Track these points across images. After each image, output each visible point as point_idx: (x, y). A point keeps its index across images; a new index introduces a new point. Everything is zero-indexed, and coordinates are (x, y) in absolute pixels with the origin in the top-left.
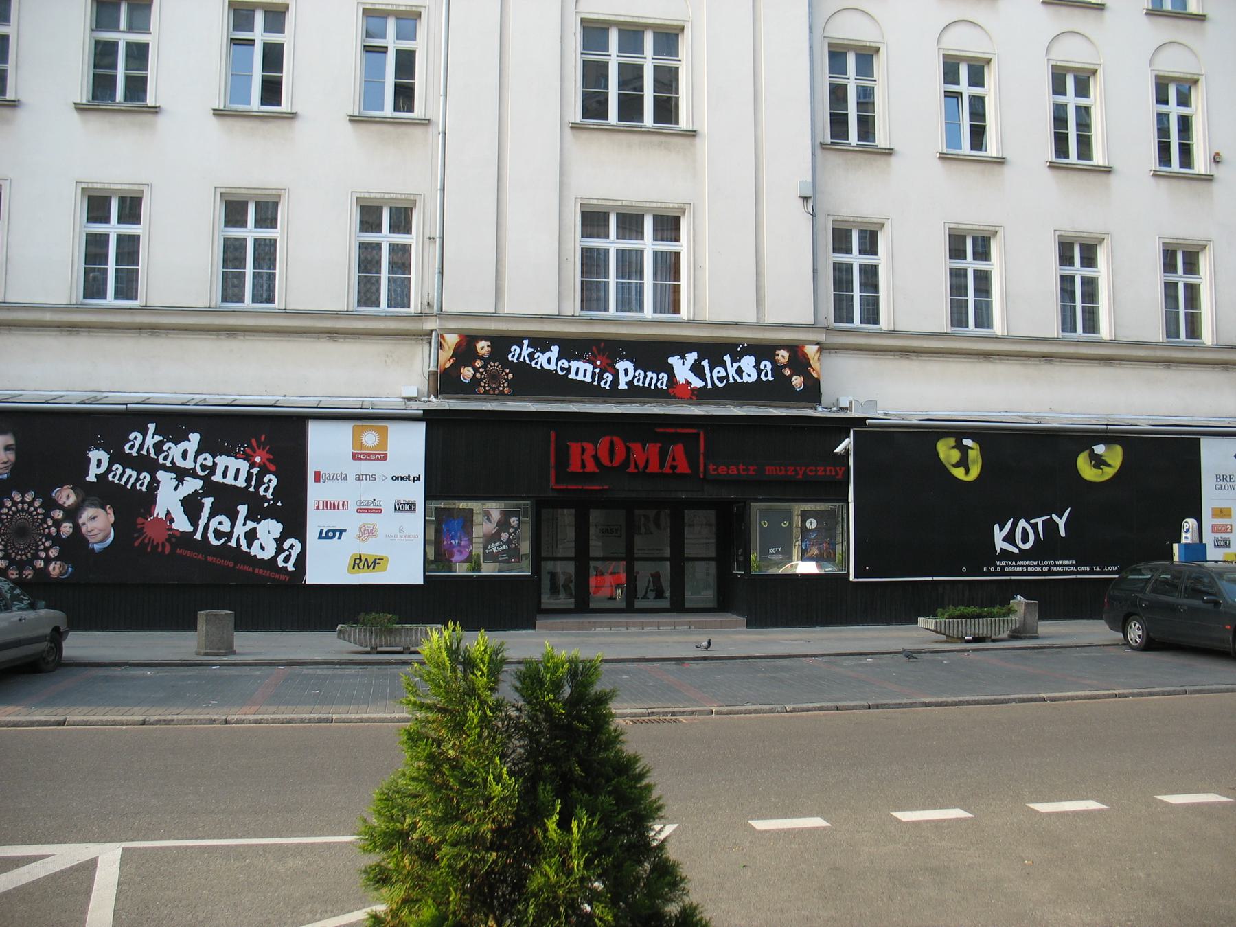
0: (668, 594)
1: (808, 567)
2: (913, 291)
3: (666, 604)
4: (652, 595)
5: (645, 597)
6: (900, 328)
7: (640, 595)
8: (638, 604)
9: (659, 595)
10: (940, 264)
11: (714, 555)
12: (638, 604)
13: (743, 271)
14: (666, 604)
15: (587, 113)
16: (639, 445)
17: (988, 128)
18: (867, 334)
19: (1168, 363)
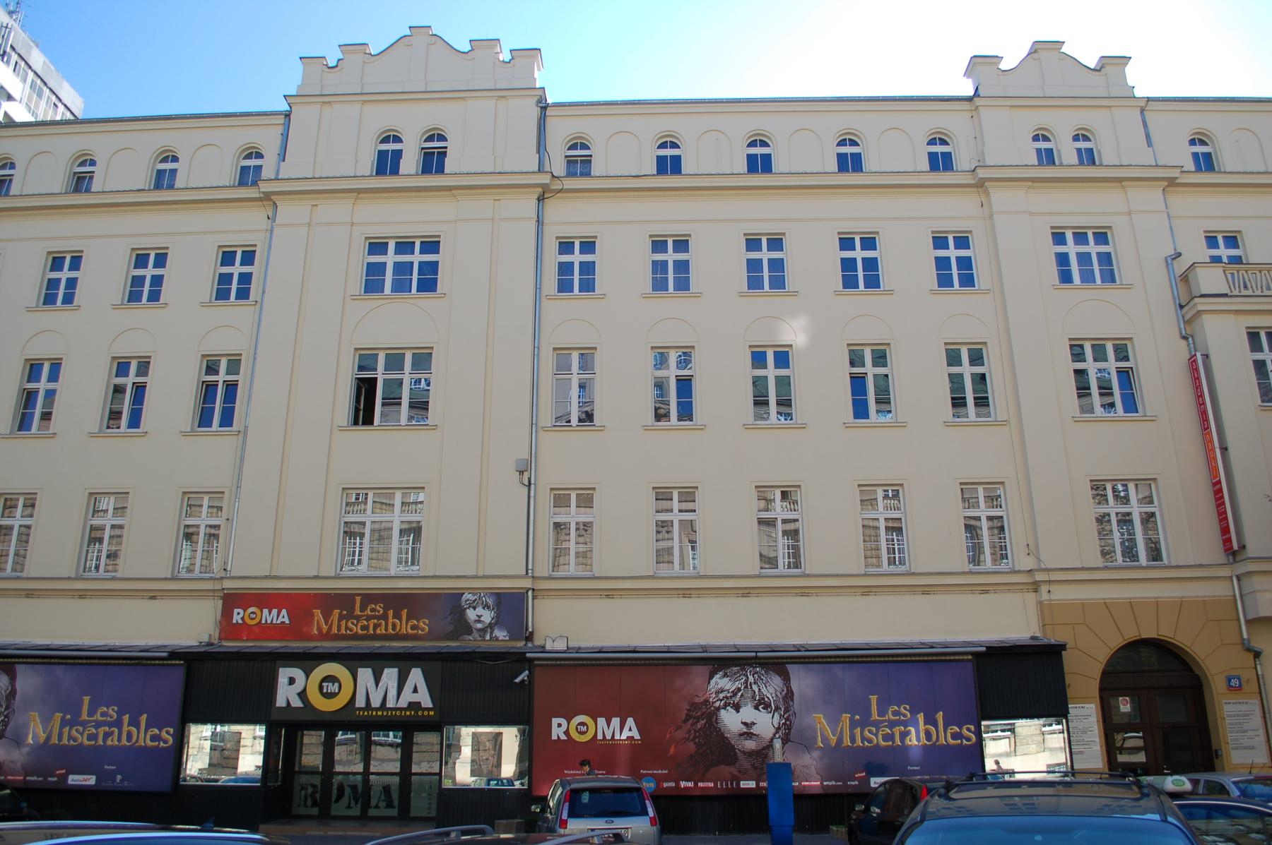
0: (396, 803)
1: (752, 784)
2: (624, 542)
3: (394, 812)
4: (382, 804)
5: (377, 807)
6: (321, 574)
7: (373, 803)
8: (372, 812)
9: (390, 805)
10: (645, 514)
11: (413, 778)
12: (372, 812)
13: (469, 543)
14: (394, 812)
15: (857, 416)
16: (293, 705)
17: (76, 296)
18: (18, 578)
19: (867, 591)
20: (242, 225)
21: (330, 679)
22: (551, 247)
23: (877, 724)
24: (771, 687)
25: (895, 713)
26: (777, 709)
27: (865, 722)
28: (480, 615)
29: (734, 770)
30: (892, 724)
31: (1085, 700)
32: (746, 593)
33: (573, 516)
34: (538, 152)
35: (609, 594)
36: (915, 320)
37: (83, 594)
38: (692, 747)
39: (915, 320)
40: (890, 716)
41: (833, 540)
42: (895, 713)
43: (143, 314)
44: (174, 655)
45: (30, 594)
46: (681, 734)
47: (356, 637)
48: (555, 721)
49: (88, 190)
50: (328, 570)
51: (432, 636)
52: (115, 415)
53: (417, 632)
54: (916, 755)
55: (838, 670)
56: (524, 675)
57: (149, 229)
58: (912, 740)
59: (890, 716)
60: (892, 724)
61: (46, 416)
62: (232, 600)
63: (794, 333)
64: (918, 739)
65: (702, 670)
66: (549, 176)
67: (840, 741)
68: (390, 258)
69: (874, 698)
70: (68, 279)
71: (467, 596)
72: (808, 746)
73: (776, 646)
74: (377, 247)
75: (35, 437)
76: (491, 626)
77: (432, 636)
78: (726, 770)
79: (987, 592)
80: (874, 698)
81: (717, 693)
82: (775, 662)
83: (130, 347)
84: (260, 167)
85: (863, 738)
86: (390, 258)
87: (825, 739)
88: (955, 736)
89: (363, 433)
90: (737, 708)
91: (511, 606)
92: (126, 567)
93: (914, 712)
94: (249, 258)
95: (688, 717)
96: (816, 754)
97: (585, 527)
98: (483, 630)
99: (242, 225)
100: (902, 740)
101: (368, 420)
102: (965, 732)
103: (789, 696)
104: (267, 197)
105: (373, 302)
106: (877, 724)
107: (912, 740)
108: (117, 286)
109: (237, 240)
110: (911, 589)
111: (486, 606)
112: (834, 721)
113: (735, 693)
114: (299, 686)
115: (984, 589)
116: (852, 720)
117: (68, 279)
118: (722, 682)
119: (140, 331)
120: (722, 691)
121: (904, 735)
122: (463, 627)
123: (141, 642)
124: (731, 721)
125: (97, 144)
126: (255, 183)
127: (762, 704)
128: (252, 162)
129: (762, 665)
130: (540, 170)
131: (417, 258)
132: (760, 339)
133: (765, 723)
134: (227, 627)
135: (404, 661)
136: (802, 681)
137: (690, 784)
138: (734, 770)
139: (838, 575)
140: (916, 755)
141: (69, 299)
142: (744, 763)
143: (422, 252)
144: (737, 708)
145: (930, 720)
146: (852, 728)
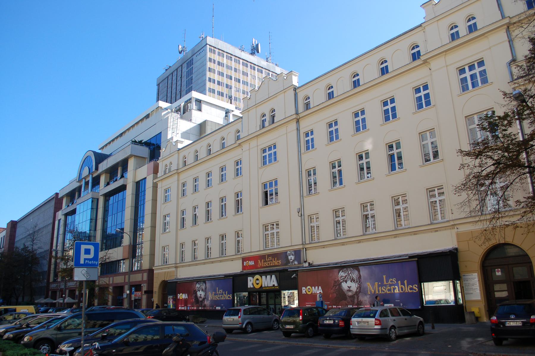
19: (396, 236)
20: (419, 76)
21: (257, 279)
22: (302, 136)
23: (386, 285)
24: (355, 275)
25: (392, 281)
26: (357, 281)
27: (382, 285)
28: (291, 257)
29: (346, 302)
30: (390, 285)
31: (474, 272)
32: (359, 241)
33: (314, 224)
34: (500, 10)
35: (324, 247)
36: (408, 127)
37: (221, 261)
38: (335, 294)
39: (408, 127)
40: (390, 282)
41: (384, 219)
42: (392, 281)
43: (393, 124)
44: (227, 276)
45: (212, 262)
46: (332, 291)
47: (267, 267)
48: (303, 288)
49: (310, 108)
50: (262, 249)
51: (282, 265)
52: (335, 183)
53: (278, 264)
54: (397, 296)
55: (373, 267)
56: (294, 275)
57: (385, 91)
58: (397, 291)
59: (390, 282)
60: (390, 285)
61: (401, 164)
62: (244, 259)
63: (368, 146)
64: (399, 291)
65: (336, 270)
66: (508, 18)
67: (375, 291)
68: (468, 74)
69: (384, 276)
70: (391, 108)
71: (288, 252)
72: (366, 294)
73: (345, 262)
74: (462, 71)
75: (433, 163)
76: (294, 260)
77: (282, 265)
78: (344, 302)
79: (437, 231)
80: (384, 276)
81: (341, 277)
82: (355, 266)
83: (334, 157)
84: (419, 51)
85: (382, 291)
86: (468, 74)
87: (371, 291)
88: (411, 289)
89: (267, 207)
90: (346, 282)
91: (297, 253)
92: (379, 228)
93: (397, 281)
94: (426, 87)
95: (334, 285)
96: (368, 296)
97: (405, 208)
98: (292, 262)
99: (419, 76)
100: (394, 291)
101: (267, 203)
102: (414, 287)
103: (360, 277)
104: (425, 62)
105: (467, 95)
106: (386, 285)
107: (397, 291)
108: (412, 104)
109: (419, 83)
110: (410, 233)
111: (292, 255)
112: (373, 285)
113: (345, 277)
114: (252, 282)
115: (436, 230)
116: (378, 284)
117: (391, 108)
118: (342, 274)
119: (393, 131)
120: (342, 276)
121: (394, 289)
122: (288, 262)
123: (192, 276)
124: (345, 286)
125: (331, 80)
126: (419, 58)
127: (353, 280)
128: (416, 50)
129: (352, 267)
130: (503, 17)
131: (477, 70)
132: (358, 150)
133: (354, 287)
134: (244, 267)
135: (270, 273)
136: (364, 272)
137: (351, 306)
138: (346, 302)
139: (383, 232)
140: (397, 296)
141: (394, 116)
142: (349, 299)
143: (479, 67)
144: (346, 282)
145: (403, 284)
146: (378, 287)
